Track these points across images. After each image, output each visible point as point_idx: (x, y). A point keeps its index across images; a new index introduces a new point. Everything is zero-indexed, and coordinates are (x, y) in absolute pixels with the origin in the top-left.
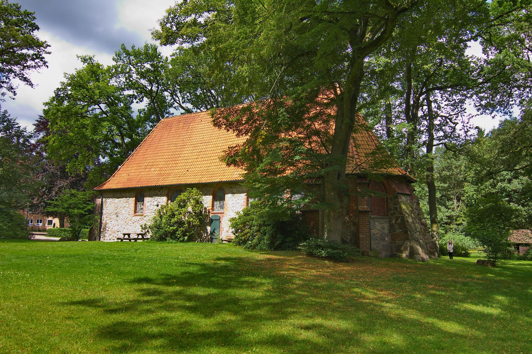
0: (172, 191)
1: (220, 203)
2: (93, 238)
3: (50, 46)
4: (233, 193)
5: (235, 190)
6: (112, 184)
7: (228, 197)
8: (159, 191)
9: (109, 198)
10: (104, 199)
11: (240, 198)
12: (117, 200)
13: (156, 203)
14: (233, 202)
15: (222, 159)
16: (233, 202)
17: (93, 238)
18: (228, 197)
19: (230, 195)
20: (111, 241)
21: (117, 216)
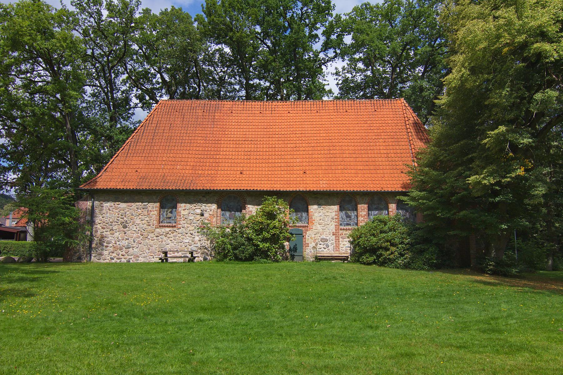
0: (231, 200)
1: (296, 215)
2: (75, 258)
3: (296, 245)
4: (319, 204)
5: (321, 201)
6: (106, 180)
7: (313, 208)
8: (204, 196)
9: (108, 201)
10: (96, 203)
11: (330, 211)
12: (123, 205)
13: (199, 211)
14: (320, 214)
15: (219, 261)
16: (320, 214)
17: (75, 258)
18: (313, 208)
19: (316, 207)
20: (113, 261)
21: (125, 227)
